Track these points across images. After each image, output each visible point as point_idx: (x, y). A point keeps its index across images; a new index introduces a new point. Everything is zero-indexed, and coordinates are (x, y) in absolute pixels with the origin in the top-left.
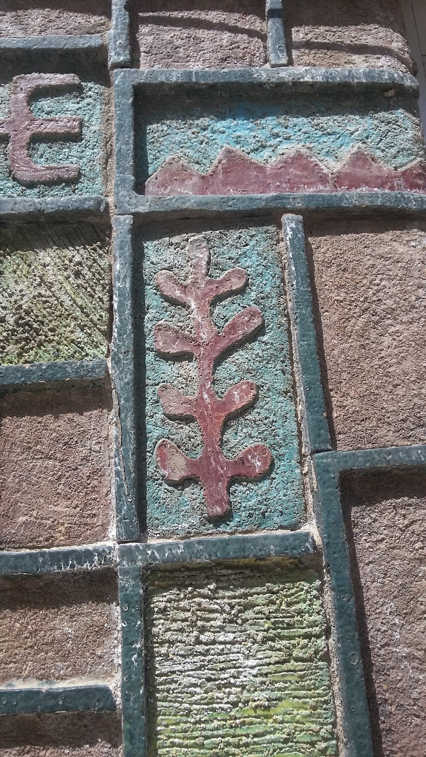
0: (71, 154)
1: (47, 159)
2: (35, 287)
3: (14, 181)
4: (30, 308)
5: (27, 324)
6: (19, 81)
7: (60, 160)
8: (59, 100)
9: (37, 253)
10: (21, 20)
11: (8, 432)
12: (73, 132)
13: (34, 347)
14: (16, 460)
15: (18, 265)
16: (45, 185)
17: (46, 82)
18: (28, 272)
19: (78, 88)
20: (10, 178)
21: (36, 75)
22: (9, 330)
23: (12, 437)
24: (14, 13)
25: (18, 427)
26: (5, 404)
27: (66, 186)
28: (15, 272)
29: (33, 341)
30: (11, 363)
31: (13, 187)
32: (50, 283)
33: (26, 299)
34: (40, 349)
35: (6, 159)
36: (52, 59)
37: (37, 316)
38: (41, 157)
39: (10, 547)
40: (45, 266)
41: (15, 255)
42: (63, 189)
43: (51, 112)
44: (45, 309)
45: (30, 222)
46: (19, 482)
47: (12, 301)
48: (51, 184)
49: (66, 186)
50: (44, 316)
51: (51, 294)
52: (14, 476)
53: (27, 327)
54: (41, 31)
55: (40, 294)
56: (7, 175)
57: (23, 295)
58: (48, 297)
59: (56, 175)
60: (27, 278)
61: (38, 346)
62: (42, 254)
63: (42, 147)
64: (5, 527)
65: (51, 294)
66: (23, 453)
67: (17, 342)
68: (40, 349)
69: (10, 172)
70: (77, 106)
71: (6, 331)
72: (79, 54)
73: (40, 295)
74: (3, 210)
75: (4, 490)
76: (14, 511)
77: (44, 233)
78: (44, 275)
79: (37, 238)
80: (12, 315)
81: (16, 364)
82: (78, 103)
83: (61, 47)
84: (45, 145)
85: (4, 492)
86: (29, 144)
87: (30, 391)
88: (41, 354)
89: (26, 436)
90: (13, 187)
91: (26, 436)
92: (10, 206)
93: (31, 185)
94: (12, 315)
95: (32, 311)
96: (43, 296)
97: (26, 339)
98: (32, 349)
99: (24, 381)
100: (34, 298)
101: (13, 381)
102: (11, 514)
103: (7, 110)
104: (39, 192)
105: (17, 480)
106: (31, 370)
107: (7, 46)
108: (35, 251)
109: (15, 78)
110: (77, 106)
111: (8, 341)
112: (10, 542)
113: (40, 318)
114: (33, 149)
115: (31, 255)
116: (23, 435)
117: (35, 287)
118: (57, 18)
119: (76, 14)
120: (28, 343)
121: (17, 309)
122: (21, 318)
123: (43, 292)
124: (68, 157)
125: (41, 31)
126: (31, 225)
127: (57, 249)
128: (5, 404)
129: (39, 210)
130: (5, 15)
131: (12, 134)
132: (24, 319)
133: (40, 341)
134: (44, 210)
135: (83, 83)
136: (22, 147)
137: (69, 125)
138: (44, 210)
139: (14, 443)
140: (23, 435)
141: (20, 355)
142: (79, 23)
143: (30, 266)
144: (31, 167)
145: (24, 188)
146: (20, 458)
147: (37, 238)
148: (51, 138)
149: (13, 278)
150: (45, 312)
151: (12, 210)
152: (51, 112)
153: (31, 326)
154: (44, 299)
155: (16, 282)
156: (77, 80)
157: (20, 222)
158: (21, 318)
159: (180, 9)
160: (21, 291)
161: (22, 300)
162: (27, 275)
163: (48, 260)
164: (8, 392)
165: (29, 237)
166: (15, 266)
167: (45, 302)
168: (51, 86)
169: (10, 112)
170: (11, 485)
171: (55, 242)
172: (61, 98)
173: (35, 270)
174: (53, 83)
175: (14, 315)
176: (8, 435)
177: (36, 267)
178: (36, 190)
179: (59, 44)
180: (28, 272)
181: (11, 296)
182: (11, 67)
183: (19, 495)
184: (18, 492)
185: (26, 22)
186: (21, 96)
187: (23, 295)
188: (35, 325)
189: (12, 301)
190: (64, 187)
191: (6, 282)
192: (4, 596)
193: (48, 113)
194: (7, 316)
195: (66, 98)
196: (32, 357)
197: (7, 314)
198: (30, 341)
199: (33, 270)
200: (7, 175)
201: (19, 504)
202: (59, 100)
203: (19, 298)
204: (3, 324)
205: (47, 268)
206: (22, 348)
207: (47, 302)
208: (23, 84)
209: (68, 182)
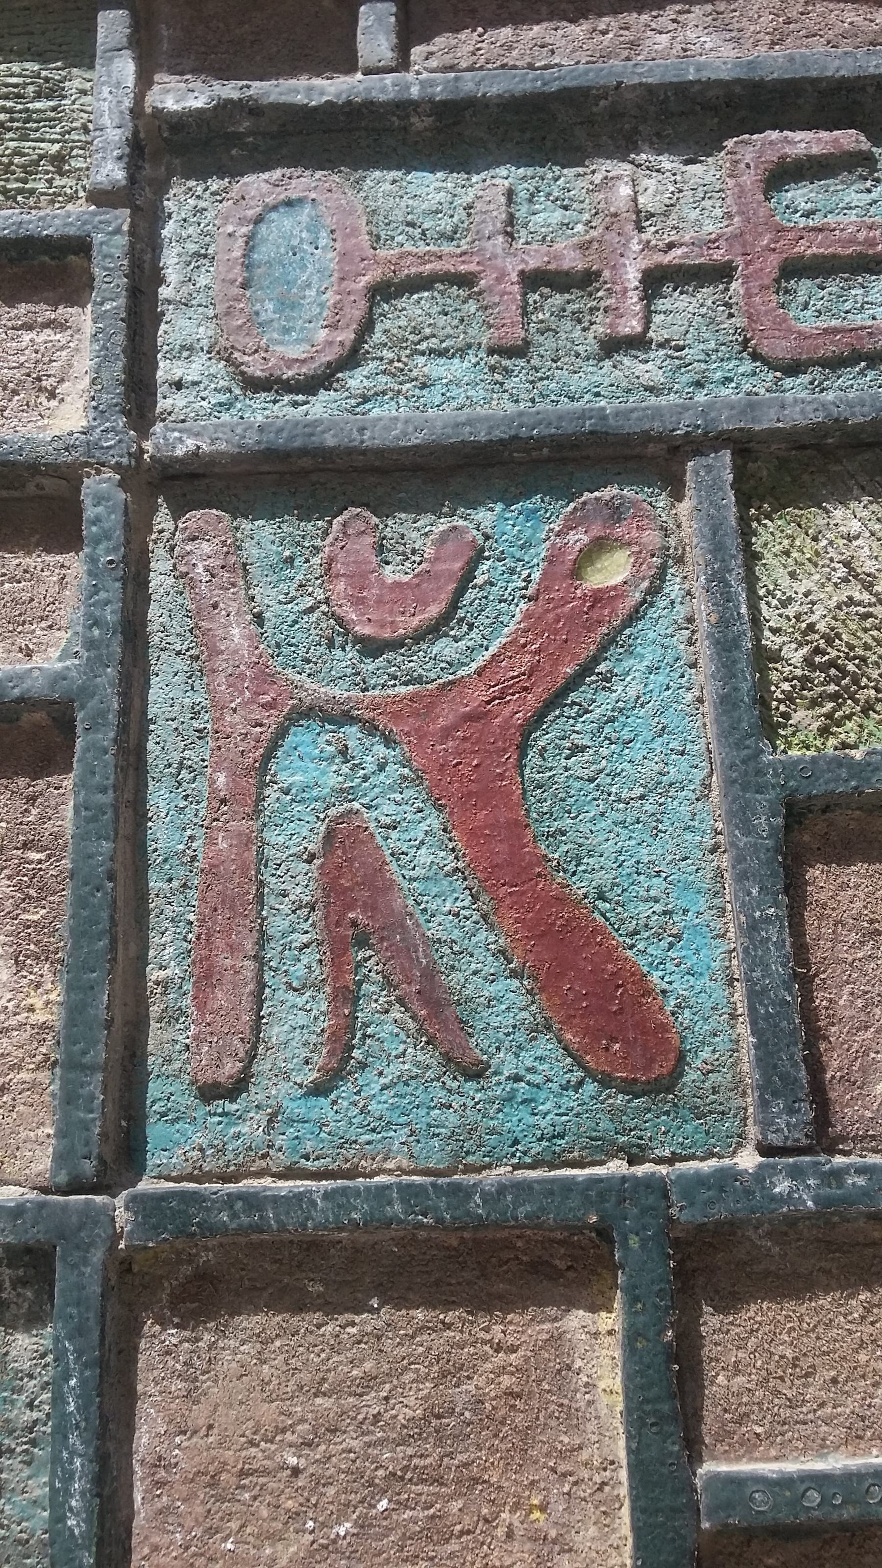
0: (869, 299)
1: (819, 312)
2: (836, 584)
3: (754, 361)
4: (832, 629)
5: (832, 664)
6: (740, 149)
7: (847, 312)
8: (829, 186)
9: (827, 512)
10: (727, 21)
11: (823, 897)
12: (870, 252)
13: (854, 714)
14: (850, 959)
15: (792, 538)
16: (823, 367)
17: (800, 150)
18: (817, 553)
19: (866, 159)
20: (745, 354)
21: (774, 135)
22: (794, 678)
23: (833, 909)
24: (709, 7)
25: (844, 886)
26: (806, 838)
27: (868, 367)
28: (787, 553)
29: (849, 702)
30: (808, 748)
31: (754, 374)
32: (869, 575)
33: (819, 610)
34: (868, 717)
35: (731, 316)
36: (801, 101)
37: (852, 648)
38: (806, 306)
39: (866, 1149)
40: (849, 538)
41: (780, 518)
42: (862, 373)
43: (813, 212)
44: (866, 630)
45: (804, 447)
46: (865, 1006)
47: (791, 615)
48: (835, 364)
49: (868, 367)
50: (867, 647)
51: (874, 600)
52: (852, 994)
53: (833, 671)
54: (773, 43)
55: (850, 598)
56: (738, 348)
57: (813, 603)
58: (870, 605)
59: (847, 344)
60: (816, 565)
61: (862, 712)
62: (839, 513)
63: (804, 287)
64: (847, 1105)
65: (874, 600)
66: (862, 943)
67: (814, 703)
68: (868, 717)
69: (746, 341)
70: (868, 197)
71: (786, 680)
72: (863, 89)
73: (851, 602)
74: (760, 422)
75: (833, 1024)
76: (863, 1070)
77: (837, 468)
78: (853, 558)
79: (823, 479)
80: (794, 646)
81: (818, 750)
82: (869, 191)
83: (830, 74)
84: (809, 282)
85: (833, 1029)
86: (777, 281)
87: (858, 809)
88: (871, 728)
89: (865, 907)
90: (754, 374)
91: (865, 907)
92: (773, 413)
93: (794, 368)
94: (794, 646)
95: (838, 636)
96: (859, 604)
97: (834, 697)
98: (849, 717)
99: (856, 788)
100: (839, 607)
101: (832, 786)
102: (856, 1076)
103: (718, 212)
104: (811, 383)
105: (859, 1003)
106: (869, 764)
107: (713, 77)
108: (825, 509)
109: (730, 143)
110: (868, 197)
111: (792, 700)
112: (864, 1137)
113: (860, 652)
114: (787, 291)
115: (815, 518)
116: (859, 904)
117: (836, 584)
118: (802, 14)
119: (842, 5)
120: (840, 706)
121: (804, 633)
122: (817, 651)
123: (857, 596)
124: (862, 307)
125: (773, 43)
126: (808, 452)
127: (871, 502)
128: (806, 838)
129: (837, 420)
130: (689, 12)
131: (739, 261)
132: (824, 653)
133: (867, 702)
134: (847, 420)
135: (874, 149)
136: (763, 287)
137: (861, 236)
138: (847, 420)
139: (841, 922)
140: (859, 904)
141: (824, 732)
142: (851, 23)
143: (815, 539)
144: (790, 330)
145: (778, 374)
146: (860, 955)
147: (823, 479)
148: (820, 268)
149: (785, 567)
150: (867, 638)
151: (779, 421)
152: (813, 212)
153: (842, 670)
154: (862, 610)
155: (793, 575)
156: (865, 145)
157: (783, 446)
158: (817, 651)
159: (294, 66)
160: (806, 595)
161: (812, 612)
162: (815, 559)
163: (855, 526)
164: (810, 811)
165: (806, 477)
166: (786, 542)
167: (866, 616)
168: (810, 157)
169: (729, 215)
170: (847, 1013)
171: (863, 488)
172: (831, 181)
173: (830, 549)
174: (815, 150)
175: (800, 645)
176: (825, 904)
177: (831, 543)
178: (804, 379)
179: (826, 68)
180: (817, 553)
181: (785, 604)
182: (716, 120)
183: (869, 1034)
184: (866, 1028)
185: (737, 26)
186: (749, 179)
187: (813, 603)
188: (851, 667)
189: (791, 615)
190: (865, 369)
191: (769, 576)
192: (875, 1257)
193: (807, 215)
194: (785, 648)
195: (842, 182)
196: (852, 735)
197: (784, 644)
198: (845, 700)
199: (825, 547)
200: (738, 348)
201: (873, 1055)
202: (829, 186)
203: (805, 608)
204: (778, 666)
205: (855, 543)
206: (829, 716)
207: (866, 616)
208: (748, 155)
209: (872, 360)
